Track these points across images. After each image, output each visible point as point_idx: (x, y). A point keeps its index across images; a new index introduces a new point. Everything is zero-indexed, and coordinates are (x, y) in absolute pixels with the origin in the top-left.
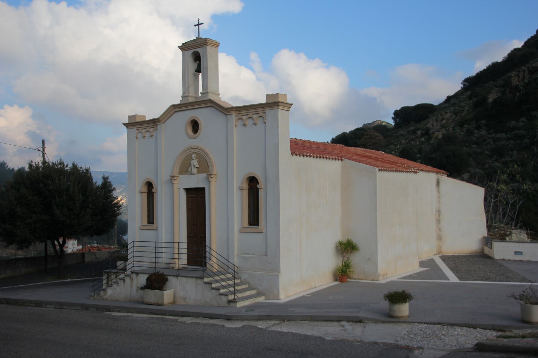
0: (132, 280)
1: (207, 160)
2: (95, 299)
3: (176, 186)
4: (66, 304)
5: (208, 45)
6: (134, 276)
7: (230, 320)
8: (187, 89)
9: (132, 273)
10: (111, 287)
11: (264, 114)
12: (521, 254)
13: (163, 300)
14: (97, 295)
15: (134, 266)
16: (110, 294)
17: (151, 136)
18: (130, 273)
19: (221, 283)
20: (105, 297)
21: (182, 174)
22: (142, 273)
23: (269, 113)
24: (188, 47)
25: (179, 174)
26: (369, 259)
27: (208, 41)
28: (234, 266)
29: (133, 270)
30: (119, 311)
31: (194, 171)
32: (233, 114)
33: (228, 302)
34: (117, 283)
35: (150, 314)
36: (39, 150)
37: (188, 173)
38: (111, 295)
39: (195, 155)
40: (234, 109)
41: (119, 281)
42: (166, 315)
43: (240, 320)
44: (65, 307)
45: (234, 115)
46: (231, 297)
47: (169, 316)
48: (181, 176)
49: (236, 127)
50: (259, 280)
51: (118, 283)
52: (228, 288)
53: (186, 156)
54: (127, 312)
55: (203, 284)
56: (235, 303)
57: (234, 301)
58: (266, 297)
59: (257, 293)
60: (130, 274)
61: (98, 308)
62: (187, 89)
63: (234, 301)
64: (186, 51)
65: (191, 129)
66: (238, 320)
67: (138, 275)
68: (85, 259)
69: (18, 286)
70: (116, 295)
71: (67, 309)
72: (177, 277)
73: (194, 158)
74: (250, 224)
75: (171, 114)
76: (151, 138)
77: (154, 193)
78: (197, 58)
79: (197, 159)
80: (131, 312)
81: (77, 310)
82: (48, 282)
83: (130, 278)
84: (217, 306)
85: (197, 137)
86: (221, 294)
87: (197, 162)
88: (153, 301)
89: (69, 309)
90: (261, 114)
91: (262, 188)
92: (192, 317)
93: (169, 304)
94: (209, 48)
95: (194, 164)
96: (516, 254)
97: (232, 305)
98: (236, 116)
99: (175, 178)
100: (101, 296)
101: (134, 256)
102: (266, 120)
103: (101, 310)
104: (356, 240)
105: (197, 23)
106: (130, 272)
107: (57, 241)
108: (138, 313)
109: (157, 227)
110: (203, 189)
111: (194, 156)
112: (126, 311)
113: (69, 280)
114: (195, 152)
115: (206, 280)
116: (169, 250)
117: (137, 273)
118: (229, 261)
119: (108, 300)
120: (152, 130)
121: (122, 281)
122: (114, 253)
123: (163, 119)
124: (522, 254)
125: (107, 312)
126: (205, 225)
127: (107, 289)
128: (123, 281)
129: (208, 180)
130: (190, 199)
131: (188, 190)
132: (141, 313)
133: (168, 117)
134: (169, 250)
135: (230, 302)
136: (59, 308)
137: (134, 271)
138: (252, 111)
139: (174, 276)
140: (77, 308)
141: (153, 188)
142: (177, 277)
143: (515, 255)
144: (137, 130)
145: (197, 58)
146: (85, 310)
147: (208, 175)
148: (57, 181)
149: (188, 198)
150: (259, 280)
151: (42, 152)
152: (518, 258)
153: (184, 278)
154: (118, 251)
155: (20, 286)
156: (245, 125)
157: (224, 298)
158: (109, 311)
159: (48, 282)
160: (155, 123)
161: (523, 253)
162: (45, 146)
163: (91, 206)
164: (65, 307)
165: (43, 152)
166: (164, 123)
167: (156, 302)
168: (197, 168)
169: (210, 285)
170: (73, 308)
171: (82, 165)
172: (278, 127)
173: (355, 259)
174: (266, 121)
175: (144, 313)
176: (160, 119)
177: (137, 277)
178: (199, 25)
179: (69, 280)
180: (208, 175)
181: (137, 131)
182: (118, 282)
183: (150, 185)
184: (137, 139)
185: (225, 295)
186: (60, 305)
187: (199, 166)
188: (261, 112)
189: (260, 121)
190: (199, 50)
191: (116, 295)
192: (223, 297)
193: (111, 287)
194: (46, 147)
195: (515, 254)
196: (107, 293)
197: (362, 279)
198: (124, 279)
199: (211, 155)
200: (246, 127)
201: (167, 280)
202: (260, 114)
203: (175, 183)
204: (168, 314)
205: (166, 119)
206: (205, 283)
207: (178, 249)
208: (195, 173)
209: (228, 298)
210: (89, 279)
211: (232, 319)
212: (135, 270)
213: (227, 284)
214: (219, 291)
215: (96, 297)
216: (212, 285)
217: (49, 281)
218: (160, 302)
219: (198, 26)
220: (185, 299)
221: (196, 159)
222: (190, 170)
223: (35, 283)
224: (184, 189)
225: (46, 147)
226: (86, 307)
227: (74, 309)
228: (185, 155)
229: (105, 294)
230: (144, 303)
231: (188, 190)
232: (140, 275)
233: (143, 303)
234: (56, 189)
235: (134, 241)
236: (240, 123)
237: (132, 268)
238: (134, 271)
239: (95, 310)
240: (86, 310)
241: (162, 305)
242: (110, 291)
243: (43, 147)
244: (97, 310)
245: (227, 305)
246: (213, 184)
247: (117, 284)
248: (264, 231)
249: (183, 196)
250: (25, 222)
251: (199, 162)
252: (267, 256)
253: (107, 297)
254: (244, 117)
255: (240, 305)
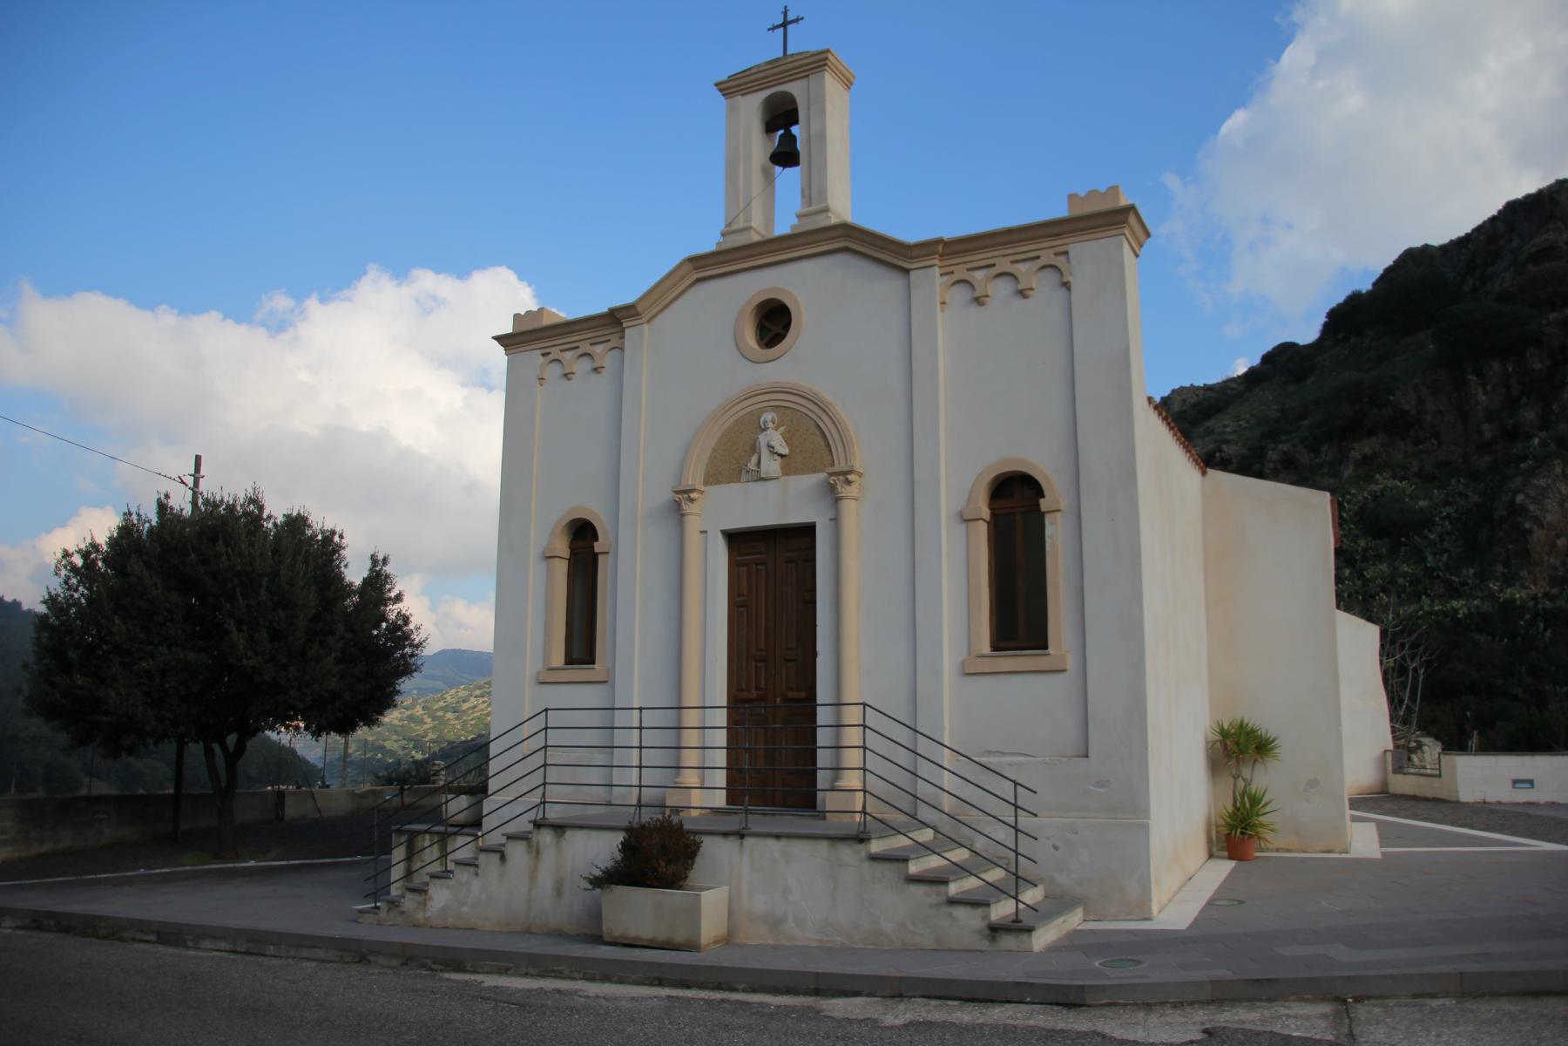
0: (537, 853)
1: (825, 429)
2: (379, 924)
3: (693, 525)
4: (279, 938)
5: (827, 68)
6: (546, 837)
7: (1081, 1006)
8: (744, 209)
9: (538, 825)
10: (449, 878)
11: (1062, 259)
12: (1528, 785)
13: (699, 928)
14: (389, 909)
15: (544, 803)
16: (442, 904)
17: (596, 370)
18: (531, 827)
19: (945, 855)
20: (420, 916)
21: (719, 483)
22: (582, 827)
23: (1085, 253)
24: (747, 83)
25: (707, 483)
26: (1313, 783)
27: (830, 57)
28: (1016, 784)
29: (540, 816)
30: (501, 971)
31: (771, 466)
32: (934, 265)
33: (987, 932)
34: (470, 864)
35: (651, 984)
36: (183, 482)
37: (744, 476)
38: (444, 909)
39: (774, 414)
40: (940, 248)
41: (482, 857)
42: (733, 989)
43: (1125, 1005)
44: (271, 949)
45: (937, 271)
46: (1002, 910)
47: (744, 991)
48: (713, 490)
49: (942, 310)
50: (1056, 848)
51: (476, 866)
52: (979, 873)
53: (736, 421)
54: (543, 975)
55: (867, 865)
56: (1024, 937)
57: (1018, 927)
58: (1086, 911)
59: (1045, 897)
60: (530, 832)
61: (409, 957)
62: (742, 207)
63: (1018, 927)
64: (742, 95)
65: (754, 334)
66: (1115, 1004)
67: (564, 832)
68: (286, 809)
69: (93, 876)
70: (465, 909)
71: (281, 957)
72: (742, 836)
73: (770, 425)
74: (996, 647)
75: (683, 286)
76: (595, 376)
77: (600, 558)
78: (781, 116)
79: (782, 429)
80: (559, 975)
81: (323, 961)
82: (188, 868)
83: (530, 846)
84: (935, 950)
85: (783, 355)
86: (952, 902)
87: (780, 437)
88: (645, 931)
89: (288, 957)
90: (1047, 257)
91: (1059, 511)
92: (870, 995)
93: (716, 942)
94: (830, 83)
95: (772, 443)
96: (1517, 785)
97: (1008, 942)
98: (942, 275)
99: (693, 495)
100: (403, 913)
101: (545, 765)
102: (1071, 274)
103: (423, 966)
104: (1265, 721)
105: (780, 21)
106: (530, 822)
107: (220, 745)
108: (591, 978)
109: (611, 670)
110: (808, 531)
111: (768, 416)
112: (533, 971)
113: (252, 863)
114: (772, 403)
115: (876, 846)
116: (667, 738)
117: (559, 828)
118: (917, 776)
119: (431, 927)
120: (599, 349)
121: (495, 857)
122: (364, 795)
123: (680, 281)
124: (1532, 787)
125: (448, 971)
126: (814, 654)
127: (430, 885)
128: (497, 856)
129: (832, 495)
130: (745, 569)
131: (735, 539)
132: (606, 978)
133: (666, 302)
134: (667, 738)
135: (995, 930)
136: (248, 953)
137: (544, 818)
138: (1011, 251)
139: (725, 835)
140: (320, 953)
141: (596, 539)
142: (742, 836)
143: (1514, 790)
144: (544, 355)
145: (781, 116)
146: (356, 962)
147: (831, 474)
148: (243, 546)
149: (734, 566)
150: (1056, 848)
151: (193, 476)
152: (1522, 796)
153: (772, 842)
154: (373, 792)
155: (99, 876)
156: (979, 301)
157: (969, 919)
158: (460, 968)
159: (188, 868)
160: (618, 323)
161: (1535, 782)
162: (202, 473)
163: (341, 628)
164: (272, 947)
165: (196, 490)
166: (648, 321)
167: (662, 936)
168: (782, 456)
169: (901, 865)
170: (304, 953)
171: (321, 519)
172: (1123, 292)
173: (1265, 778)
174: (1071, 279)
175: (621, 981)
176: (640, 308)
177: (558, 842)
178: (785, 25)
179: (252, 863)
180: (831, 474)
181: (542, 360)
182: (477, 863)
183: (582, 534)
184: (541, 385)
185: (975, 903)
186: (253, 943)
187: (791, 450)
188: (1051, 251)
189: (1044, 285)
190: (794, 88)
191: (465, 909)
192: (962, 913)
193: (448, 881)
194: (203, 477)
195: (1514, 787)
196: (429, 903)
197: (1288, 851)
198: (503, 849)
199: (839, 409)
200: (983, 308)
201: (697, 846)
202: (1042, 258)
203: (692, 514)
204: (740, 987)
205: (660, 307)
206: (874, 858)
207: (643, 750)
208: (775, 475)
209: (986, 917)
210: (307, 861)
211: (1088, 1002)
212: (546, 816)
213: (945, 862)
214: (942, 888)
215: (382, 914)
216: (907, 866)
217: (189, 865)
218: (679, 937)
219: (782, 29)
220: (775, 923)
221: (779, 426)
222: (752, 465)
223: (147, 868)
224: (724, 532)
225: (203, 477)
226: (359, 953)
227: (308, 959)
228: (735, 418)
229: (424, 904)
230: (606, 938)
231: (735, 539)
232: (569, 834)
233: (599, 940)
234: (239, 567)
235: (546, 710)
236: (960, 295)
237: (538, 805)
238: (544, 818)
239: (395, 962)
240: (360, 961)
241: (692, 946)
242: (440, 896)
243: (197, 475)
244: (403, 964)
245: (984, 944)
246: (849, 509)
247: (472, 869)
248: (1071, 663)
249: (720, 555)
250: (135, 668)
251: (788, 439)
252: (1087, 756)
253: (428, 914)
254: (979, 276)
255: (1044, 937)
